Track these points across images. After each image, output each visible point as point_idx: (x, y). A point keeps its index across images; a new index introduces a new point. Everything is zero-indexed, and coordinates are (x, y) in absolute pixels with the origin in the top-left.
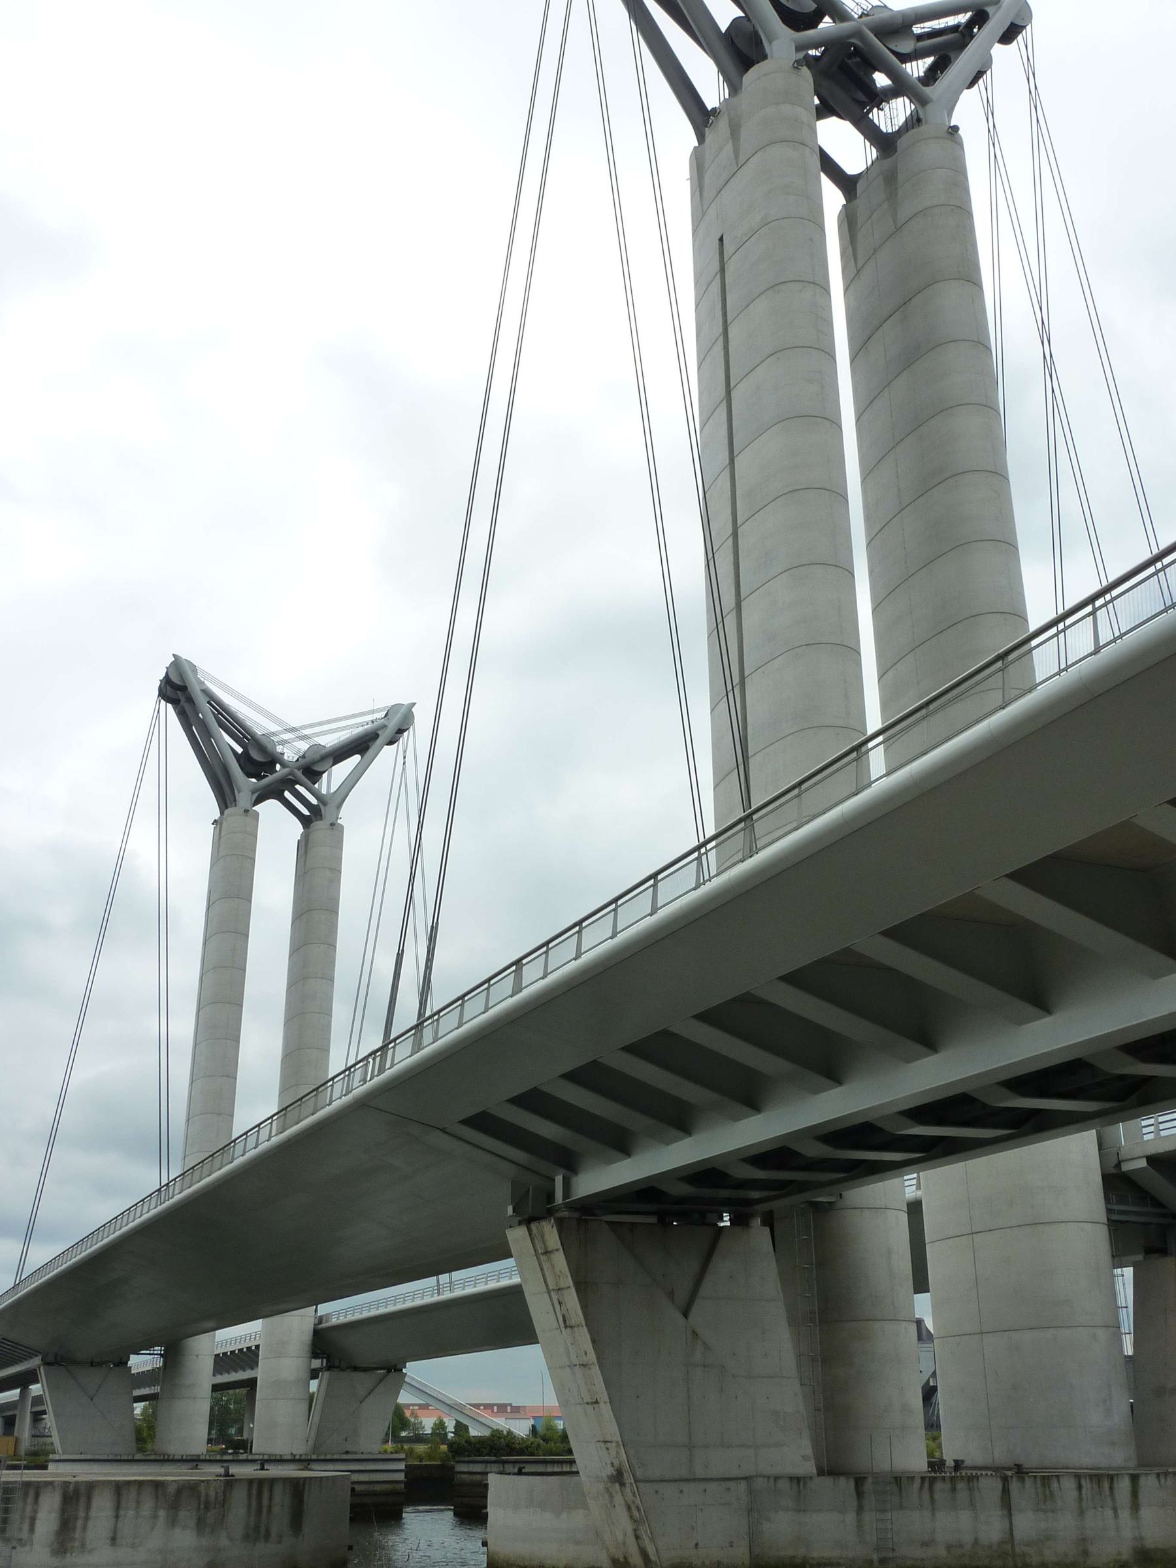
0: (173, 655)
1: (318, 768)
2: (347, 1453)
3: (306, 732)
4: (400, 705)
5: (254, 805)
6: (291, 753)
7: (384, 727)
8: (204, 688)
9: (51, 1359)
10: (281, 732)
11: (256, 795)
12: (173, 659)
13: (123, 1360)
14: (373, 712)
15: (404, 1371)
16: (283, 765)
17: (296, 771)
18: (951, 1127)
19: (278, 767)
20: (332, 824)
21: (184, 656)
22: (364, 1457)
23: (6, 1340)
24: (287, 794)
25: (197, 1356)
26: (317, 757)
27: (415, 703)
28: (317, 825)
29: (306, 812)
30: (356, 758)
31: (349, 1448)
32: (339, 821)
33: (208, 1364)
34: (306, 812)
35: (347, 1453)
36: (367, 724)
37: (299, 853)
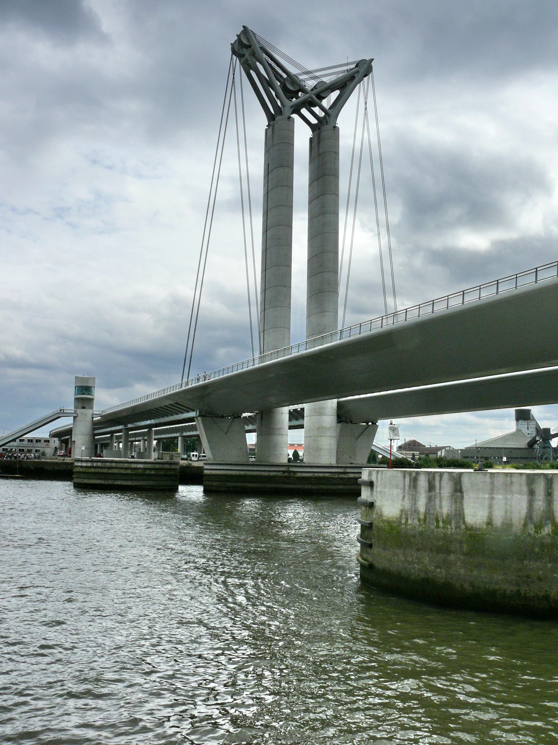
0: (244, 27)
1: (323, 95)
2: (352, 464)
3: (317, 74)
4: (364, 60)
5: (292, 114)
6: (310, 84)
7: (358, 72)
8: (261, 46)
9: (204, 413)
10: (300, 74)
11: (292, 109)
12: (243, 29)
13: (239, 415)
14: (348, 64)
15: (377, 424)
16: (304, 91)
17: (313, 96)
18: (122, 411)
19: (300, 94)
20: (335, 127)
21: (250, 28)
22: (264, 464)
23: (179, 404)
24: (304, 111)
25: (282, 414)
26: (323, 88)
27: (373, 60)
28: (325, 127)
29: (314, 121)
30: (337, 93)
31: (352, 461)
32: (336, 125)
33: (286, 417)
34: (314, 121)
35: (352, 464)
36: (344, 72)
37: (313, 145)
